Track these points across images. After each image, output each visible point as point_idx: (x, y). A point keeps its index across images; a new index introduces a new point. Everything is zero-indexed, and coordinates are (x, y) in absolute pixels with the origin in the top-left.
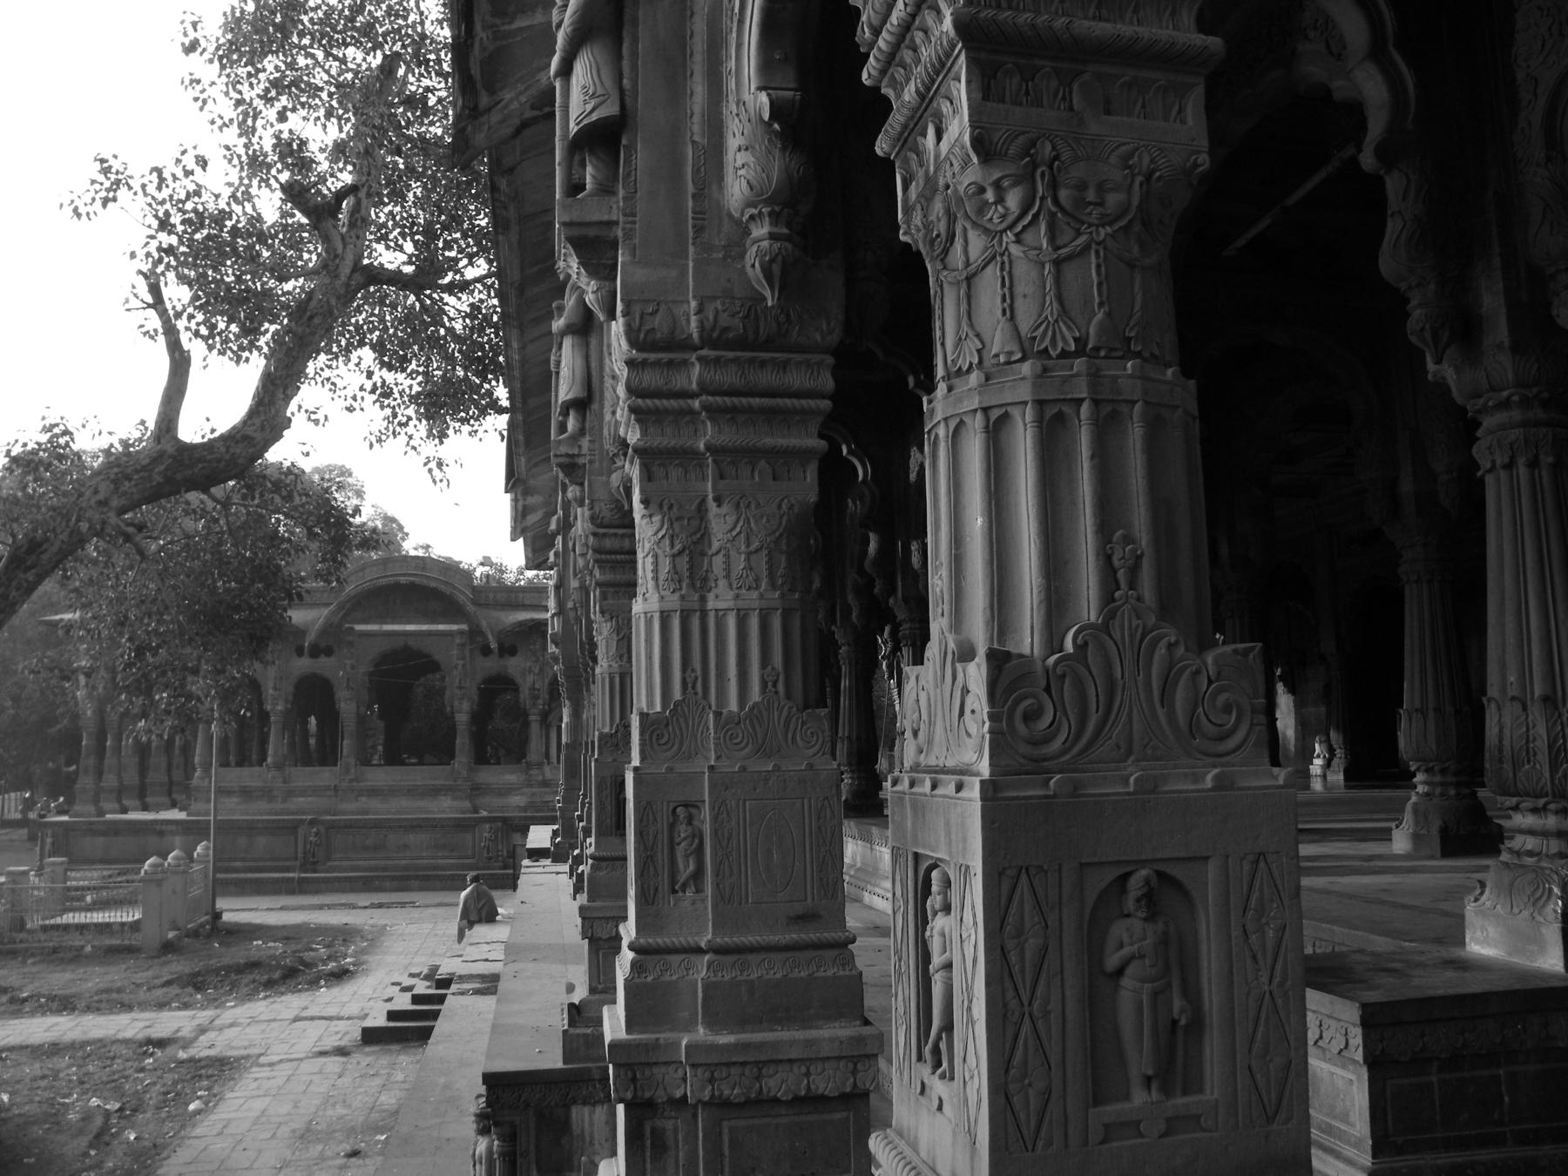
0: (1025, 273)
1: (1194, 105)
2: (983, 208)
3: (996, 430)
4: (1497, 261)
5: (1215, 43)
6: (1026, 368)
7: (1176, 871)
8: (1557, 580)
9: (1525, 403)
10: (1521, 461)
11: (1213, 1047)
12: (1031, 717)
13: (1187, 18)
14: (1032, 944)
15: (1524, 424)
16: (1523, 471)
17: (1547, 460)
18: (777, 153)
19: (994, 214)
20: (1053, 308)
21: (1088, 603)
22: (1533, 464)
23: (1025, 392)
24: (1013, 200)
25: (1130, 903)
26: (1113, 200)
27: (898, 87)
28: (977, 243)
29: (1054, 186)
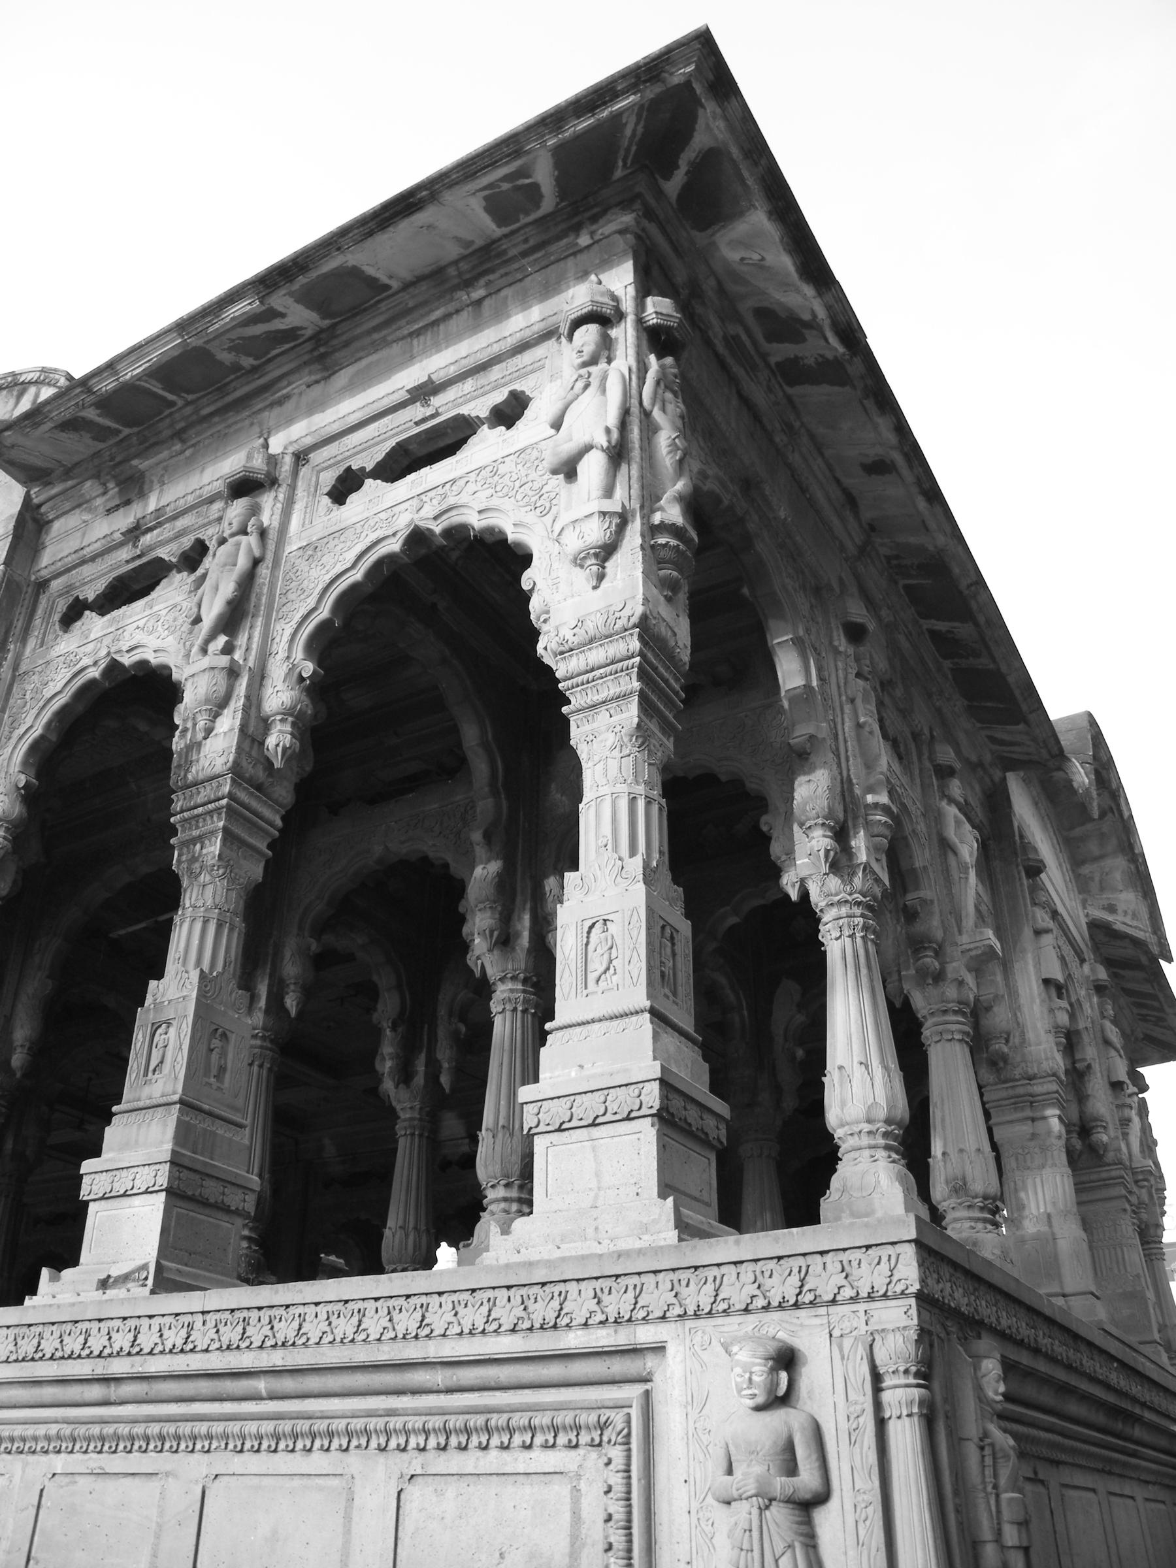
0: (219, 888)
1: (262, 865)
2: (213, 870)
3: (206, 922)
4: (268, 971)
5: (270, 853)
6: (217, 911)
7: (228, 1033)
8: (260, 1119)
9: (264, 1038)
10: (256, 1063)
11: (227, 1076)
12: (206, 986)
13: (265, 844)
14: (199, 1034)
15: (261, 1047)
16: (256, 1068)
17: (267, 1065)
18: (18, 803)
19: (215, 872)
20: (223, 900)
21: (219, 967)
22: (261, 1066)
23: (215, 916)
24: (221, 871)
25: (217, 1035)
26: (242, 880)
27: (184, 831)
28: (208, 878)
29: (231, 872)
